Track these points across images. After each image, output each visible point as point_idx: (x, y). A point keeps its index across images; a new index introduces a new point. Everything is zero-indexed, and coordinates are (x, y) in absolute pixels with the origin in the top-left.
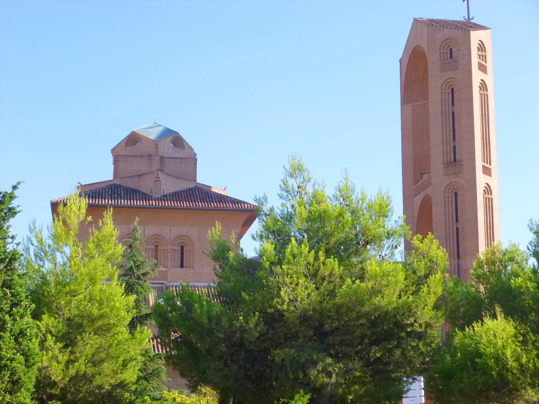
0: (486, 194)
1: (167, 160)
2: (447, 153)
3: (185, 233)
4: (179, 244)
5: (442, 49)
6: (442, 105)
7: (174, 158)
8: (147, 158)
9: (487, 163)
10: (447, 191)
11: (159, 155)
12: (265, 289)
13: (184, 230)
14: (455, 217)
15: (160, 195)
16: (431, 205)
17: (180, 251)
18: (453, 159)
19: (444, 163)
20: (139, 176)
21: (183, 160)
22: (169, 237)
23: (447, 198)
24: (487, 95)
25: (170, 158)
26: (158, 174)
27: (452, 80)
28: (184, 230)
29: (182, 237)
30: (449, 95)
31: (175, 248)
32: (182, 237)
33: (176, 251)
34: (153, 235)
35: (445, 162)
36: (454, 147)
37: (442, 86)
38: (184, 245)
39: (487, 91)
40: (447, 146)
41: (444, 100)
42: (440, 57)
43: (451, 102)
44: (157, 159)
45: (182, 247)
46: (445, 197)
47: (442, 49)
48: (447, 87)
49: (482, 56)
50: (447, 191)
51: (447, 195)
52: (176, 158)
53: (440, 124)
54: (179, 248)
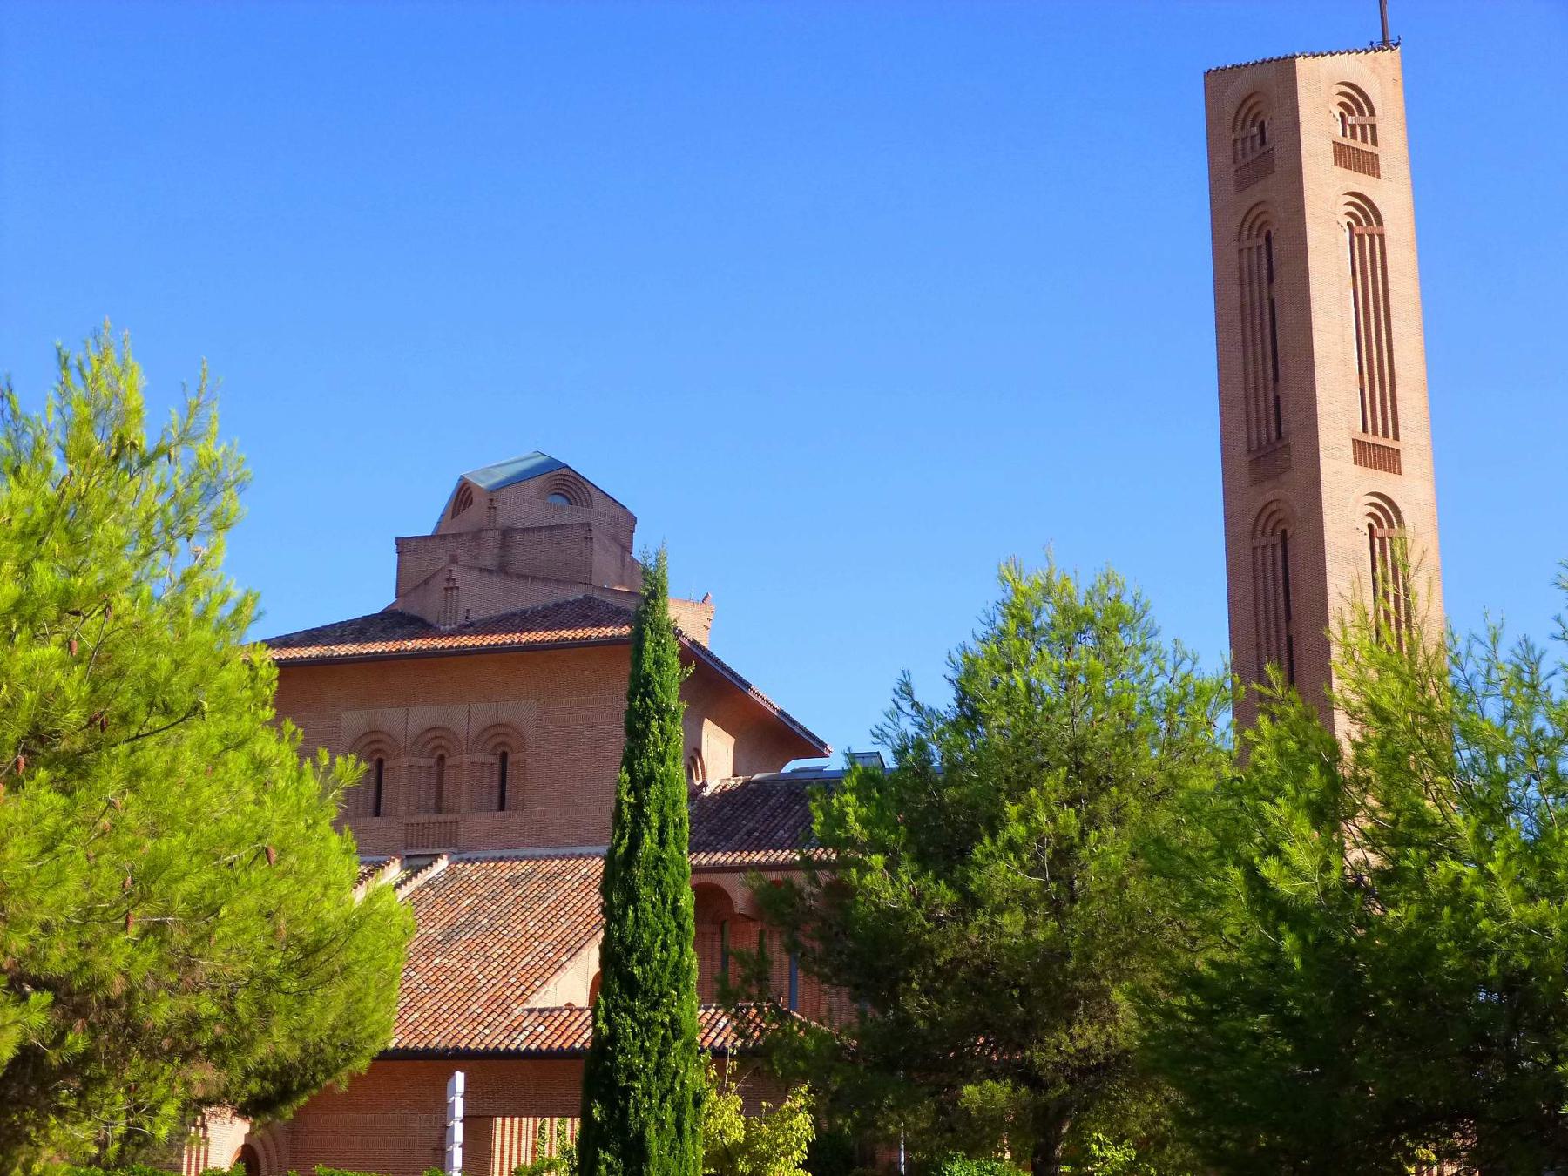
0: (1381, 525)
1: (518, 537)
2: (1258, 419)
3: (505, 719)
4: (495, 747)
5: (1239, 128)
6: (1241, 285)
7: (533, 529)
8: (470, 537)
9: (1385, 435)
10: (1259, 532)
11: (497, 526)
12: (1397, 1076)
13: (502, 711)
14: (1282, 606)
15: (455, 623)
16: (471, 493)
17: (497, 767)
18: (1274, 435)
19: (1249, 451)
20: (426, 582)
21: (557, 532)
22: (465, 733)
23: (1259, 551)
24: (1382, 237)
25: (526, 530)
26: (450, 571)
27: (1261, 208)
28: (502, 711)
29: (500, 730)
30: (1259, 255)
31: (481, 758)
32: (500, 730)
33: (486, 768)
34: (429, 730)
35: (1255, 447)
36: (1277, 399)
37: (1240, 232)
38: (507, 749)
39: (1380, 222)
40: (1257, 401)
41: (1246, 270)
42: (1235, 154)
43: (1265, 272)
44: (492, 537)
45: (504, 756)
46: (1255, 549)
47: (1239, 128)
48: (1254, 232)
49: (1363, 127)
50: (1259, 532)
51: (1261, 542)
52: (540, 528)
53: (1239, 339)
54: (496, 760)
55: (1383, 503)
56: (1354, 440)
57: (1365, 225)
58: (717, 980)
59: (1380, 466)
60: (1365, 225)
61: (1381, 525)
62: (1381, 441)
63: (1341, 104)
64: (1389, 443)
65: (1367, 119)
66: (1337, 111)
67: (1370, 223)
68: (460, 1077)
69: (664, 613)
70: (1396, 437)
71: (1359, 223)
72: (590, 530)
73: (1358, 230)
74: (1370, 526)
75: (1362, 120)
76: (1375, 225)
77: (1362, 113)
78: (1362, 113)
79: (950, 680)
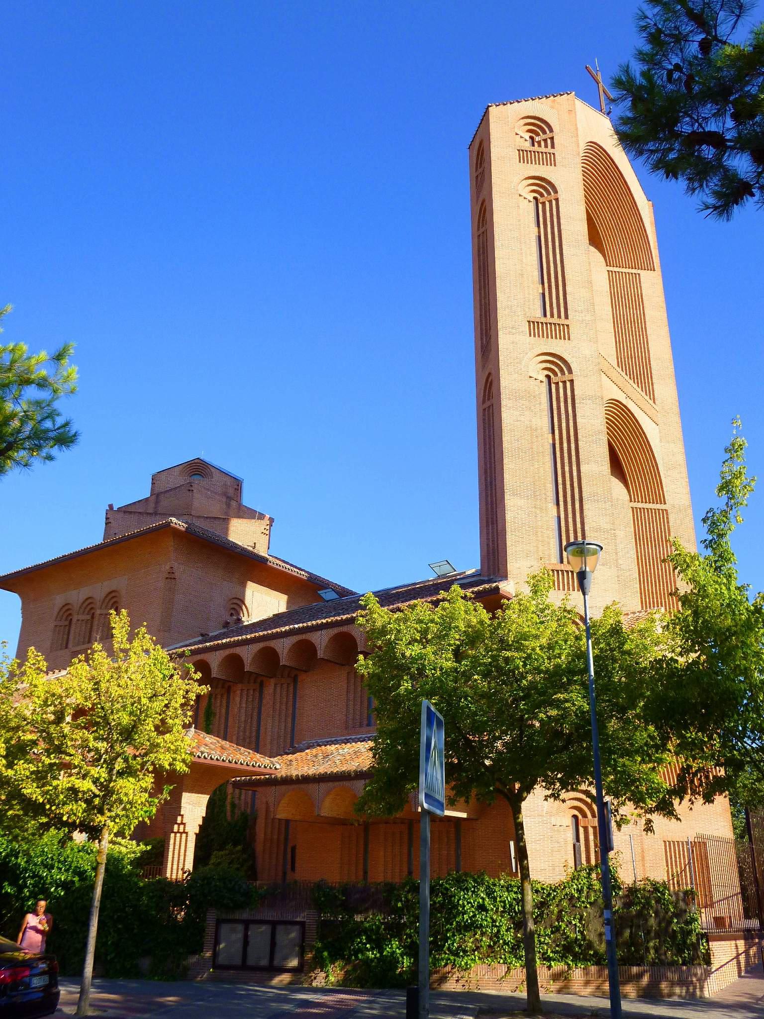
24: (557, 200)
55: (555, 360)
56: (529, 322)
57: (546, 195)
58: (377, 888)
59: (657, 501)
60: (546, 195)
61: (556, 374)
62: (555, 320)
63: (529, 131)
64: (563, 321)
65: (549, 134)
66: (527, 136)
67: (549, 193)
68: (464, 815)
69: (43, 938)
70: (567, 317)
71: (542, 195)
72: (618, 577)
73: (541, 200)
74: (548, 377)
75: (544, 137)
76: (552, 193)
77: (544, 132)
78: (544, 132)
79: (584, 594)
